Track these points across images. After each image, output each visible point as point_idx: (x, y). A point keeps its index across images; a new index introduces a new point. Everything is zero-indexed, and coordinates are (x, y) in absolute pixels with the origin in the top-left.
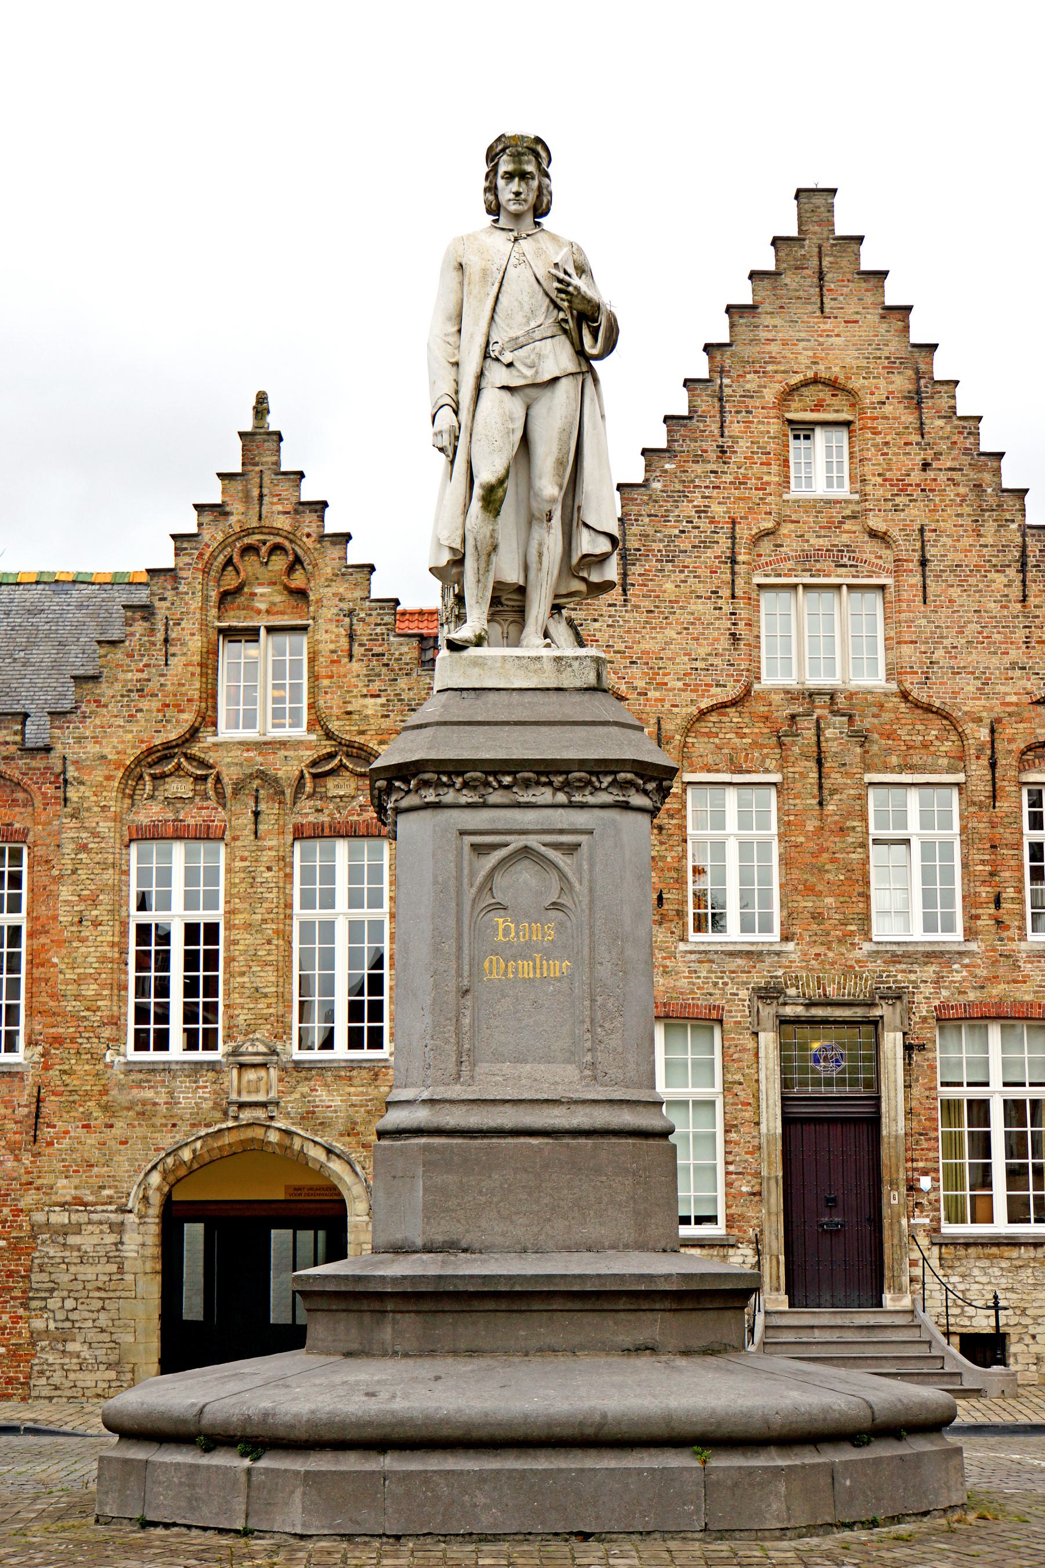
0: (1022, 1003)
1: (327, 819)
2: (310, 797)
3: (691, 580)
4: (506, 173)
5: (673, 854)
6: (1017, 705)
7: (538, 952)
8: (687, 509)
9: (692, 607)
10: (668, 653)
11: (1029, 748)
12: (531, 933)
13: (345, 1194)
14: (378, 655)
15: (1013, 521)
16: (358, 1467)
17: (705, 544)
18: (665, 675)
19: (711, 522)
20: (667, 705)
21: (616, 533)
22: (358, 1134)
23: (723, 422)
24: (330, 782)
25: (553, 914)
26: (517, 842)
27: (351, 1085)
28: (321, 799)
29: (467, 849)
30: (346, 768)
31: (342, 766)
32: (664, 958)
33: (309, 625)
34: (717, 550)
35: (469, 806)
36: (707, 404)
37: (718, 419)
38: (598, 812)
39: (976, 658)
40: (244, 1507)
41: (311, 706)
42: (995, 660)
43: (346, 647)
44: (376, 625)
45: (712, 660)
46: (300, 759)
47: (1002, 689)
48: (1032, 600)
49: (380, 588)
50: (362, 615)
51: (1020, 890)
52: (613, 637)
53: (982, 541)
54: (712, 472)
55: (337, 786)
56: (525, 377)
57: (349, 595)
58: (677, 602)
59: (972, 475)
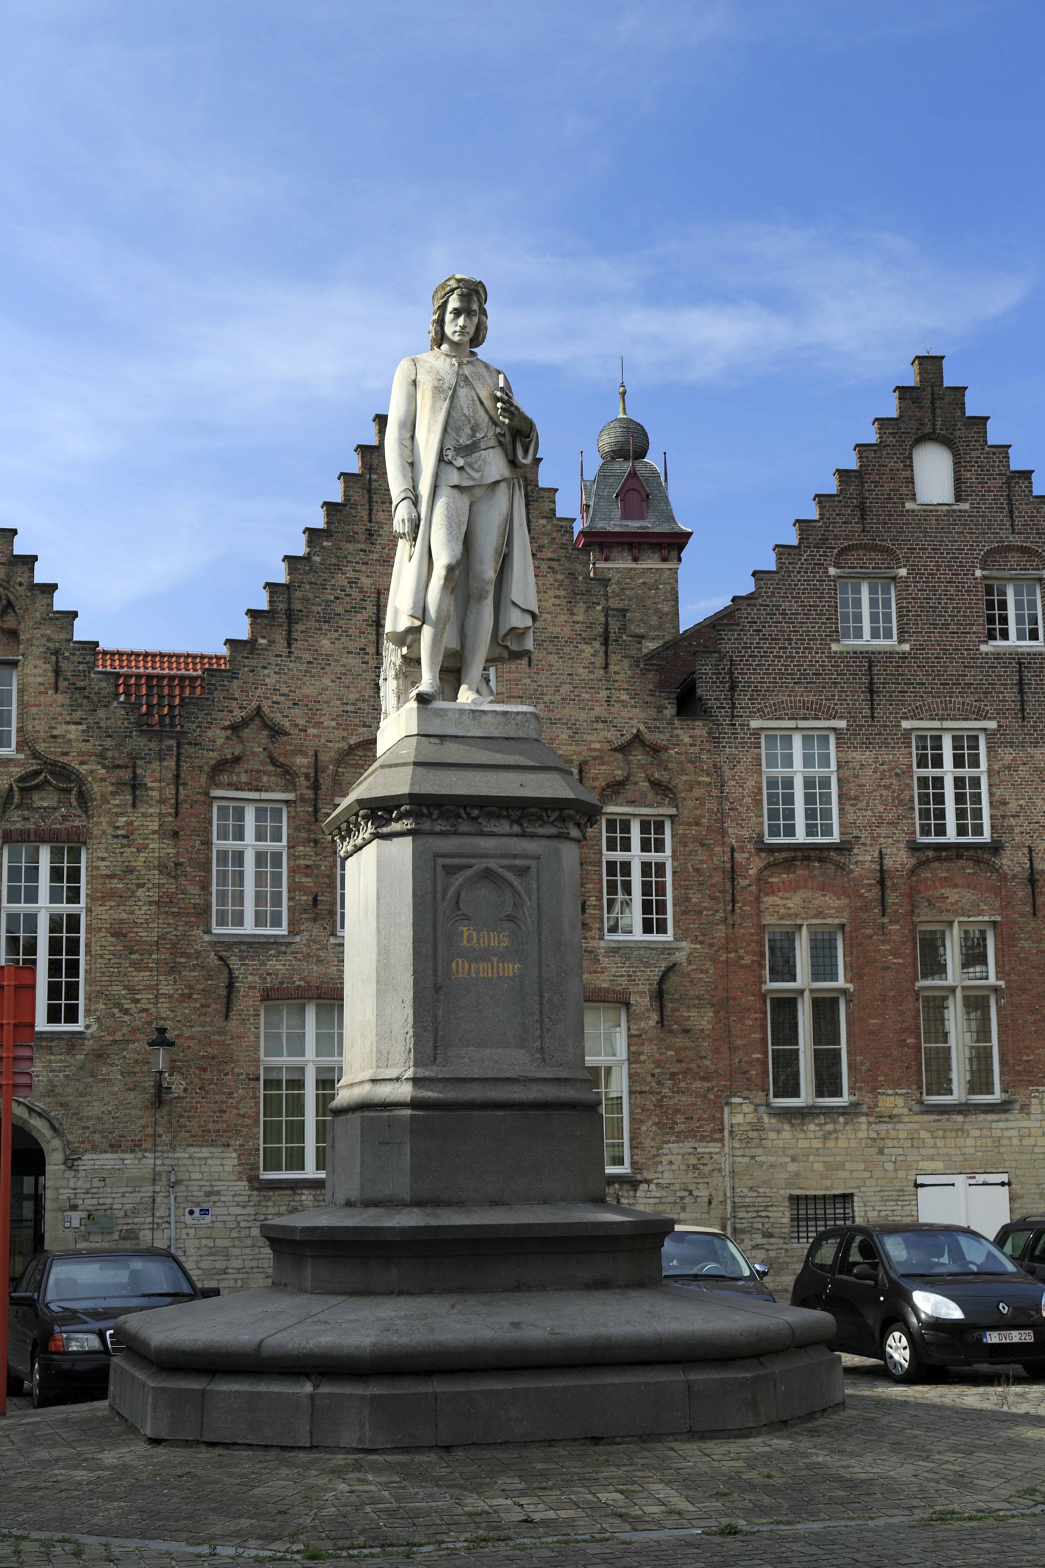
0: (601, 989)
1: (32, 827)
2: (18, 807)
3: (343, 639)
4: (455, 309)
5: (326, 863)
6: (599, 750)
7: (495, 955)
8: (341, 580)
9: (344, 661)
10: (324, 698)
11: (609, 786)
12: (489, 940)
13: (44, 1145)
14: (80, 689)
15: (598, 604)
16: (412, 1391)
17: (356, 609)
18: (321, 715)
19: (360, 592)
20: (323, 741)
21: (537, 611)
22: (56, 1095)
23: (371, 510)
24: (36, 796)
25: (506, 924)
26: (480, 864)
27: (52, 1054)
28: (28, 809)
29: (439, 869)
30: (50, 784)
31: (46, 781)
32: (318, 949)
33: (19, 661)
34: (365, 615)
35: (442, 833)
36: (358, 496)
37: (367, 507)
38: (544, 842)
39: (568, 711)
40: (308, 1427)
41: (20, 730)
42: (583, 715)
43: (53, 680)
44: (79, 663)
45: (360, 705)
46: (10, 775)
47: (589, 737)
48: (612, 668)
49: (80, 634)
50: (67, 654)
51: (600, 899)
52: (279, 682)
53: (575, 618)
54: (362, 550)
55: (41, 799)
56: (474, 479)
57: (55, 636)
58: (332, 656)
59: (567, 565)
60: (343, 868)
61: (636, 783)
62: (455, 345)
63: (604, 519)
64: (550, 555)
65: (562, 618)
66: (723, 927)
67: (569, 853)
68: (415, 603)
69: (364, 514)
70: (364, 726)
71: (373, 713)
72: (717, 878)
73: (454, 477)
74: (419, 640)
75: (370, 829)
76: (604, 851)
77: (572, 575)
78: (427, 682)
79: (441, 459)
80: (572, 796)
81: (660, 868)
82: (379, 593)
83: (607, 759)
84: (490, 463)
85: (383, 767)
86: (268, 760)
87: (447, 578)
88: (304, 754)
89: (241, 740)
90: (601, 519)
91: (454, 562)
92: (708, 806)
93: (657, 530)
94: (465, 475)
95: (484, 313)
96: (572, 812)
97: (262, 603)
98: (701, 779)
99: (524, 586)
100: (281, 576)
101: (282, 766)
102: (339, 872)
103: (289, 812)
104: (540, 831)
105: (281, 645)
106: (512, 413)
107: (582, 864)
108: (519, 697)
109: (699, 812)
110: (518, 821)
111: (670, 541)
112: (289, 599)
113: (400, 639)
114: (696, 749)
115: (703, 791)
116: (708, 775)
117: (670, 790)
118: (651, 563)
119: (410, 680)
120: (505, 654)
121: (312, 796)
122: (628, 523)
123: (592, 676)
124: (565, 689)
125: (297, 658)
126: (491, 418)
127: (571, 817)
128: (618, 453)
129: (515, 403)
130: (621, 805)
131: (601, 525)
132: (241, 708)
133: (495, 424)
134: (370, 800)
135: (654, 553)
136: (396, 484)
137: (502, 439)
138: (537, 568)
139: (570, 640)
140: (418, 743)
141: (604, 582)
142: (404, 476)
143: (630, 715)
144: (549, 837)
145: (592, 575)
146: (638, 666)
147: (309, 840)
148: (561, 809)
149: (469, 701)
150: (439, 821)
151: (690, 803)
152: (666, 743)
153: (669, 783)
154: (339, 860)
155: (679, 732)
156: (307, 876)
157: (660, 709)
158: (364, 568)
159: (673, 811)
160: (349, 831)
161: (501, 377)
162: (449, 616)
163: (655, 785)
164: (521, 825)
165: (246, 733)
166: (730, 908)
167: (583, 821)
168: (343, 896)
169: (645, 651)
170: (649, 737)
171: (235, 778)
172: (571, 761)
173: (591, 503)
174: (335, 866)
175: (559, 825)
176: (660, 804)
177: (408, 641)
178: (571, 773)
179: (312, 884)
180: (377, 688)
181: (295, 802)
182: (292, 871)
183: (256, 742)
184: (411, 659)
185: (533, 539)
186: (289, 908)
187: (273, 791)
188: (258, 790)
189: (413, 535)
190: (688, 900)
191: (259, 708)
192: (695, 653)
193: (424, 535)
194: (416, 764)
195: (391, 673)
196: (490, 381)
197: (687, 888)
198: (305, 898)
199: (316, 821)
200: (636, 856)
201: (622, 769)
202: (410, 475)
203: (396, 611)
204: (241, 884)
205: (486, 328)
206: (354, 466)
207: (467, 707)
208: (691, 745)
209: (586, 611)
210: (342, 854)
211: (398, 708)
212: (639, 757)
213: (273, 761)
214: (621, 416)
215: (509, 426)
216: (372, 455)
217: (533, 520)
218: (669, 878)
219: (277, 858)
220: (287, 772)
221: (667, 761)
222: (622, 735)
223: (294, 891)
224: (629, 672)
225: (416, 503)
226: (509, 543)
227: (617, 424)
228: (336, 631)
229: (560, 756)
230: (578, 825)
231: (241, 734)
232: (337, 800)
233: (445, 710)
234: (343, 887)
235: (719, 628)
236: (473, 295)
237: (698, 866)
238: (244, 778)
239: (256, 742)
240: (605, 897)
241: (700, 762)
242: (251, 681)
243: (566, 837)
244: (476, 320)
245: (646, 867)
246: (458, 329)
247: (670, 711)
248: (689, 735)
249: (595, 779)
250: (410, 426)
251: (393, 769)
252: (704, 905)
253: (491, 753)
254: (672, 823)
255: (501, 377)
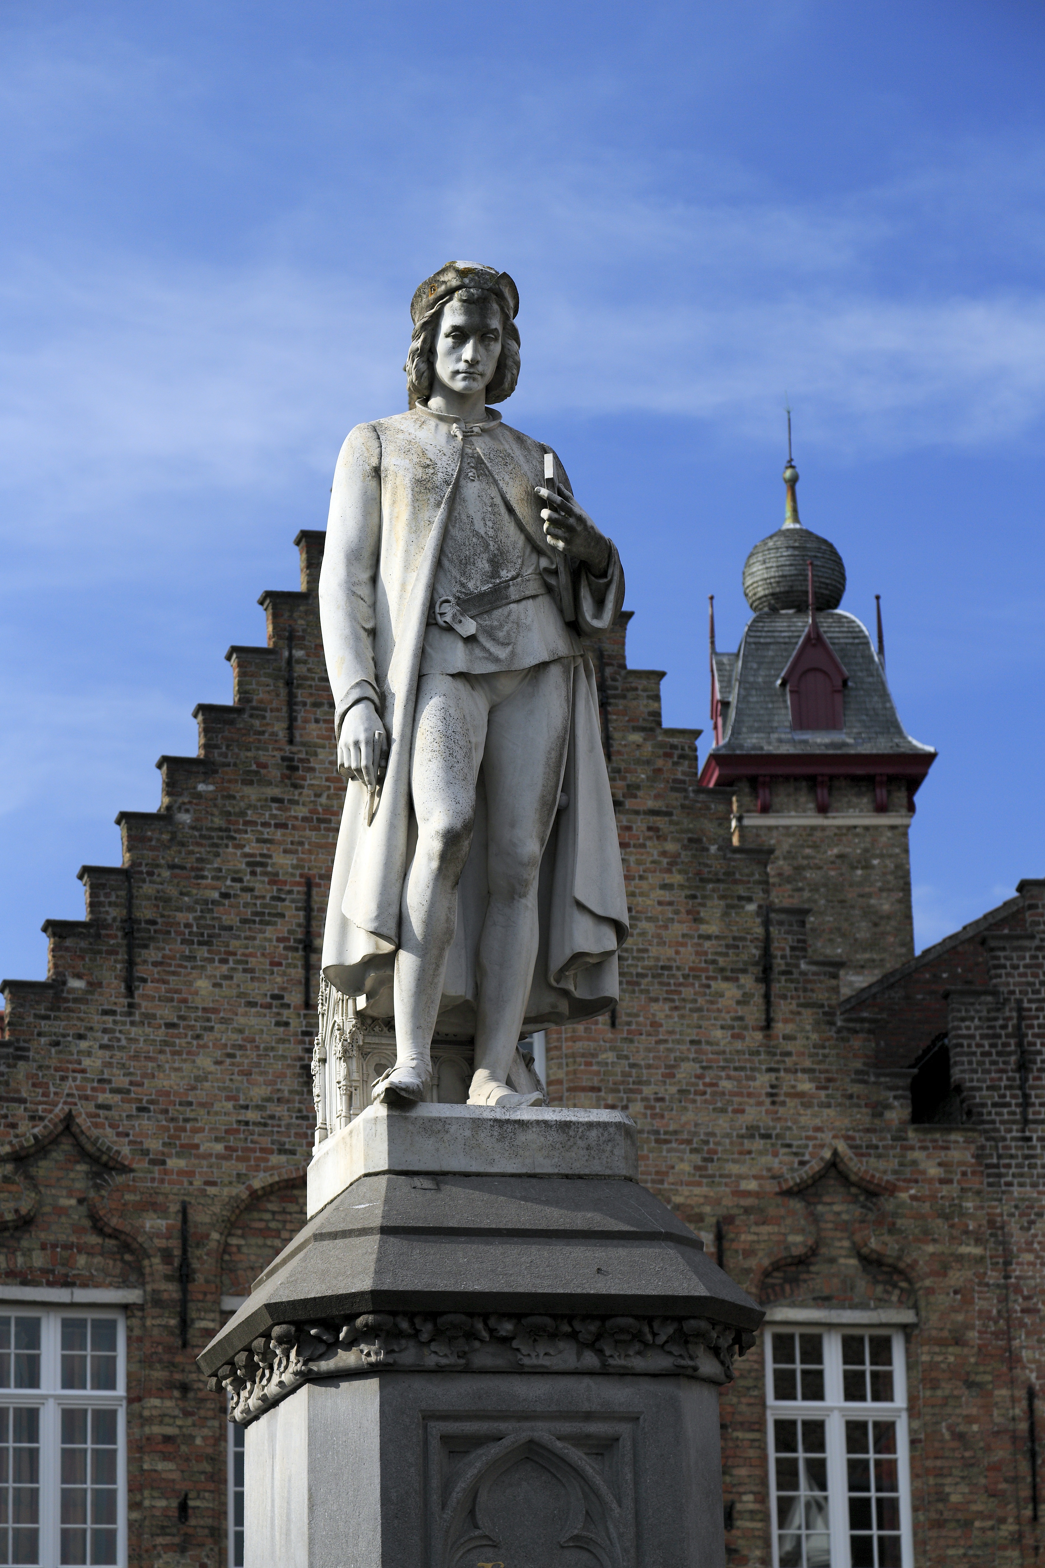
3: (238, 976)
4: (455, 328)
5: (206, 1432)
6: (757, 1195)
8: (233, 859)
10: (199, 1095)
11: (776, 1266)
15: (750, 900)
17: (263, 917)
18: (195, 1131)
19: (272, 882)
20: (198, 1182)
21: (625, 920)
23: (292, 720)
26: (516, 1433)
29: (435, 1444)
34: (282, 928)
35: (439, 1371)
36: (267, 692)
37: (284, 713)
38: (648, 1386)
39: (692, 1117)
42: (723, 1123)
48: (780, 1028)
51: (762, 1498)
52: (109, 1065)
53: (704, 929)
56: (497, 660)
58: (215, 1011)
59: (686, 823)
60: (240, 1441)
61: (832, 1261)
62: (455, 398)
63: (758, 730)
64: (650, 804)
65: (678, 929)
66: (1016, 1554)
67: (698, 1407)
68: (382, 907)
69: (280, 728)
70: (282, 1151)
71: (299, 1129)
72: (1001, 1453)
73: (458, 657)
74: (388, 982)
75: (295, 1364)
76: (770, 1400)
77: (695, 843)
78: (406, 1064)
79: (431, 621)
80: (701, 1290)
81: (885, 1433)
82: (309, 884)
83: (772, 1211)
84: (529, 628)
85: (319, 1237)
86: (87, 1223)
87: (446, 857)
88: (160, 1209)
89: (33, 1183)
90: (752, 730)
91: (459, 825)
92: (979, 1304)
93: (866, 749)
94: (478, 652)
95: (513, 334)
96: (703, 1325)
97: (75, 906)
98: (964, 1250)
99: (599, 869)
100: (113, 853)
101: (115, 1234)
102: (231, 1449)
103: (129, 1329)
104: (638, 1363)
105: (113, 990)
106: (570, 529)
107: (723, 1426)
108: (593, 1089)
109: (960, 1318)
110: (593, 1345)
111: (891, 770)
112: (130, 898)
113: (353, 979)
114: (951, 1190)
115: (969, 1274)
116: (978, 1241)
117: (900, 1272)
118: (855, 815)
119: (374, 1060)
120: (564, 1007)
121: (176, 1296)
122: (807, 736)
123: (739, 1045)
124: (686, 1071)
125: (146, 1016)
126: (529, 539)
127: (700, 1335)
128: (785, 598)
129: (577, 510)
130: (803, 1305)
131: (753, 742)
132: (32, 1118)
133: (538, 550)
134: (294, 1304)
135: (860, 794)
136: (342, 672)
137: (552, 581)
138: (624, 829)
139: (694, 974)
140: (390, 1188)
141: (759, 854)
142: (358, 655)
143: (818, 1122)
144: (654, 1375)
145: (735, 841)
146: (832, 1023)
147: (171, 1385)
148: (680, 1319)
149: (492, 1102)
150: (434, 1347)
151: (943, 1300)
152: (890, 1177)
153: (899, 1258)
154: (231, 1427)
155: (917, 1155)
156: (166, 1457)
157: (878, 1109)
158: (279, 834)
159: (908, 1317)
160: (252, 1369)
161: (549, 459)
162: (449, 932)
163: (871, 1263)
164: (600, 1352)
165: (43, 1169)
166: (1028, 1513)
167: (725, 1342)
168: (239, 1498)
169: (846, 991)
170: (856, 1166)
171: (20, 1260)
172: (699, 1218)
173: (733, 698)
174: (223, 1437)
175: (676, 1350)
176: (882, 1303)
177: (369, 983)
178: (698, 1245)
179: (176, 1476)
180: (308, 1078)
181: (141, 1307)
182: (136, 1448)
183: (63, 1187)
184: (374, 1019)
185: (615, 774)
186: (131, 1524)
187: (97, 1286)
188: (67, 1283)
189: (375, 772)
190: (943, 1498)
191: (69, 1119)
192: (946, 996)
193: (398, 772)
194: (386, 1231)
195: (335, 1048)
196: (526, 467)
197: (940, 1473)
198: (163, 1503)
199: (185, 1345)
200: (834, 1409)
201: (802, 1231)
202: (369, 654)
203: (344, 924)
204: (34, 1476)
205: (518, 365)
206: (259, 632)
207: (487, 1115)
208: (942, 1181)
209: (726, 914)
210: (238, 1414)
211: (349, 1119)
212: (837, 1207)
213: (98, 1226)
214: (789, 525)
215: (565, 553)
216: (293, 611)
217: (616, 735)
218: (902, 1454)
219: (105, 1421)
220: (126, 1247)
221: (895, 1215)
222: (802, 1163)
223: (140, 1489)
224: (814, 1036)
225: (381, 706)
226: (569, 785)
227: (780, 542)
228: (224, 961)
229: (677, 1207)
230: (716, 1351)
231: (33, 1171)
232: (228, 1303)
233: (444, 1122)
234: (240, 1480)
235: (993, 943)
236: (491, 301)
237: (962, 1428)
238: (39, 1260)
239: (63, 1187)
240: (774, 1494)
241: (962, 1215)
242: (54, 1063)
243: (692, 1375)
244: (496, 348)
245: (855, 1432)
246: (462, 366)
247: (898, 1113)
248: (937, 1162)
249: (749, 1253)
250: (368, 557)
251: (340, 1242)
252: (974, 1508)
253: (537, 1207)
254: (908, 1340)
255: (549, 459)
